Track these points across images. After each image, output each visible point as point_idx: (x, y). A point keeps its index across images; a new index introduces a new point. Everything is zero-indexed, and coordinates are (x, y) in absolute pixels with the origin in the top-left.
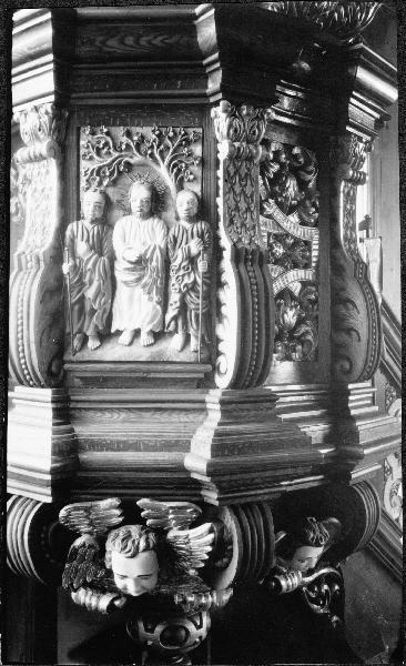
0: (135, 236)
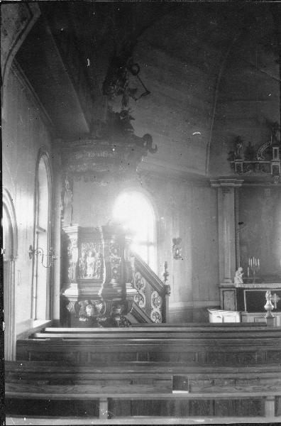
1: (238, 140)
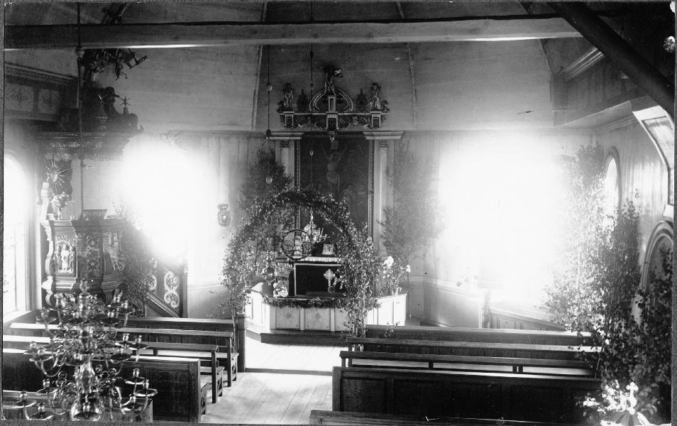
0: (65, 253)
1: (287, 88)
